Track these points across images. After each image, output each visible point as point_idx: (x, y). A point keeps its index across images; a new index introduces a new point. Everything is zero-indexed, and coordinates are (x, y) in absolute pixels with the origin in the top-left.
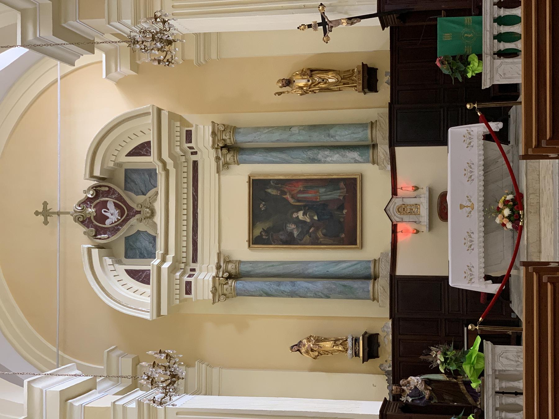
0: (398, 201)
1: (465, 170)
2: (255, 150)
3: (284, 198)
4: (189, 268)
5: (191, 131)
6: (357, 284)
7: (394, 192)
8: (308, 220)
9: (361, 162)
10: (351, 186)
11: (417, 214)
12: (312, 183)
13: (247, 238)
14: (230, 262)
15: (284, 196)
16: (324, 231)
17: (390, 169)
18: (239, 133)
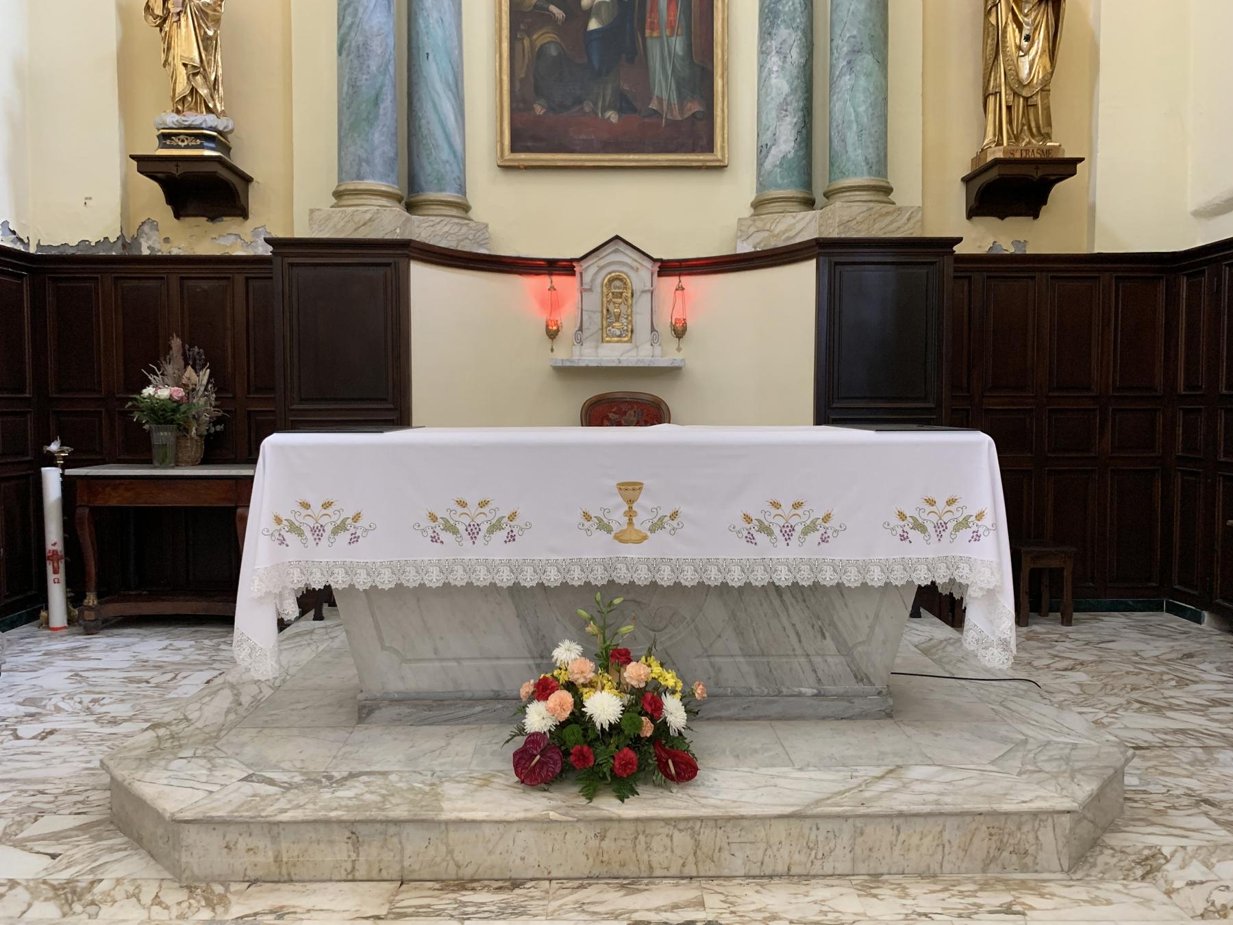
0: (642, 276)
1: (797, 505)
6: (382, 141)
7: (667, 268)
9: (760, 164)
10: (685, 135)
11: (603, 337)
16: (553, 52)
17: (739, 252)
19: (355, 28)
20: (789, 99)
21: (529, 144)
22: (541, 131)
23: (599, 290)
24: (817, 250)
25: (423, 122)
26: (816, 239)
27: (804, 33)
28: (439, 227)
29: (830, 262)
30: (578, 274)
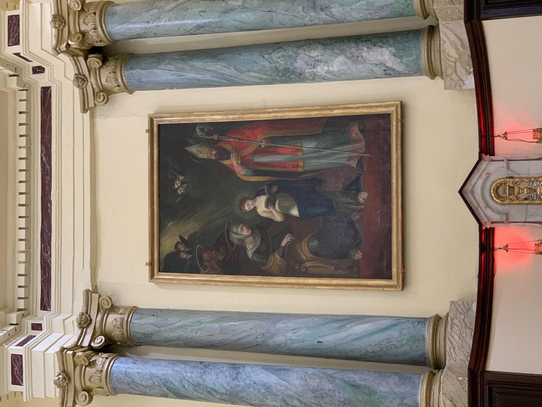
0: (495, 170)
2: (159, 57)
3: (226, 166)
4: (29, 322)
5: (17, 17)
7: (487, 147)
8: (278, 218)
9: (399, 74)
10: (377, 136)
12: (287, 129)
13: (147, 259)
14: (113, 309)
15: (226, 162)
16: (315, 243)
17: (474, 87)
18: (114, 14)
19: (301, 398)
20: (349, 55)
21: (385, 264)
22: (376, 257)
23: (507, 207)
24: (475, 21)
25: (369, 349)
26: (466, 22)
27: (299, 47)
28: (455, 343)
29: (485, 8)
30: (492, 226)
